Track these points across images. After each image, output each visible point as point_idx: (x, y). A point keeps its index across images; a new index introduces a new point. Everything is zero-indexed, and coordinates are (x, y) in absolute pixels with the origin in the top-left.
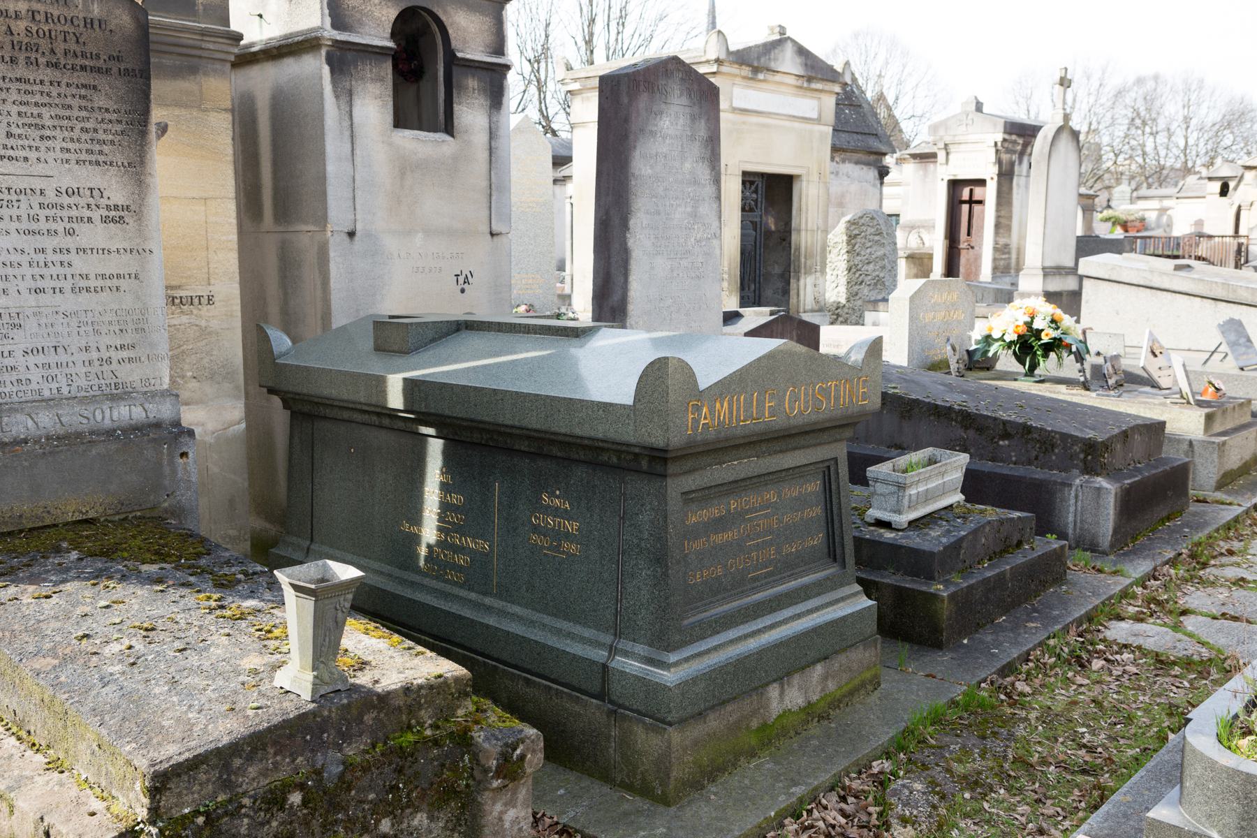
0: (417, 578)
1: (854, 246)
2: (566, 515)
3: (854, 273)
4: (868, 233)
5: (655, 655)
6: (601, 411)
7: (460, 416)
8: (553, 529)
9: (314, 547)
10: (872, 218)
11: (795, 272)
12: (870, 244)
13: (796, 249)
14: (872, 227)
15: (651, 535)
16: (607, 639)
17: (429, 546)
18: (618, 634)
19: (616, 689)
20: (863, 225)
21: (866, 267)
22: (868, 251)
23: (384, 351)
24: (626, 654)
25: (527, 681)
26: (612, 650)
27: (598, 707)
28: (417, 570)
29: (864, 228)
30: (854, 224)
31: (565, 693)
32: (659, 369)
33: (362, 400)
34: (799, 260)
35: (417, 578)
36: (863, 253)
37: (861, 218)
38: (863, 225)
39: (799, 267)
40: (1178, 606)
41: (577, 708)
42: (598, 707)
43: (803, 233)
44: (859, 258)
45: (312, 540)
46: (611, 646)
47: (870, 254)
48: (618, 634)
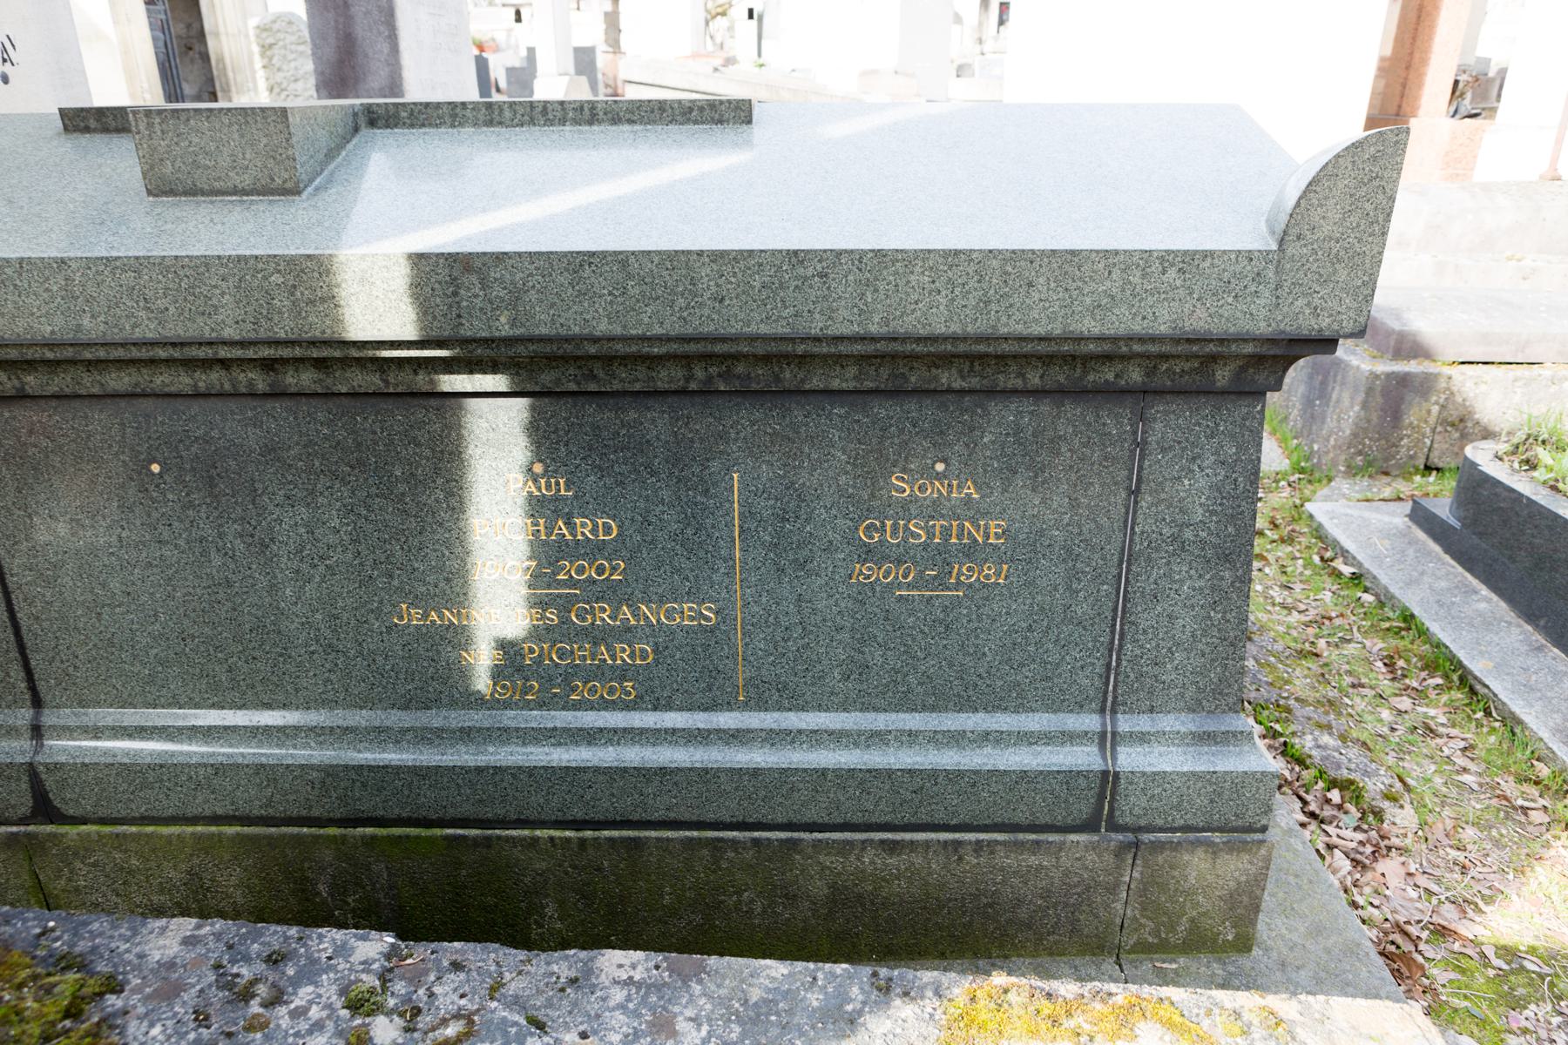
0: (477, 718)
1: (271, 59)
2: (974, 511)
3: (279, 94)
4: (287, 41)
5: (1211, 725)
6: (1172, 273)
7: (657, 330)
8: (925, 546)
9: (49, 718)
10: (290, 23)
11: (223, 90)
12: (293, 56)
13: (217, 64)
14: (293, 34)
15: (1213, 513)
16: (1090, 722)
17: (504, 645)
18: (1108, 705)
19: (1131, 807)
20: (279, 31)
21: (293, 86)
22: (293, 65)
23: (193, 192)
24: (1142, 738)
25: (892, 847)
26: (1107, 740)
27: (1094, 847)
28: (479, 701)
29: (281, 36)
30: (265, 30)
31: (1004, 843)
32: (1374, 158)
33: (229, 333)
34: (226, 75)
35: (477, 718)
36: (285, 67)
37: (274, 22)
38: (279, 31)
39: (228, 84)
40: (152, 385)
41: (1033, 860)
42: (1094, 847)
43: (223, 38)
44: (281, 74)
45: (37, 703)
46: (1103, 735)
47: (296, 69)
48: (1108, 705)
